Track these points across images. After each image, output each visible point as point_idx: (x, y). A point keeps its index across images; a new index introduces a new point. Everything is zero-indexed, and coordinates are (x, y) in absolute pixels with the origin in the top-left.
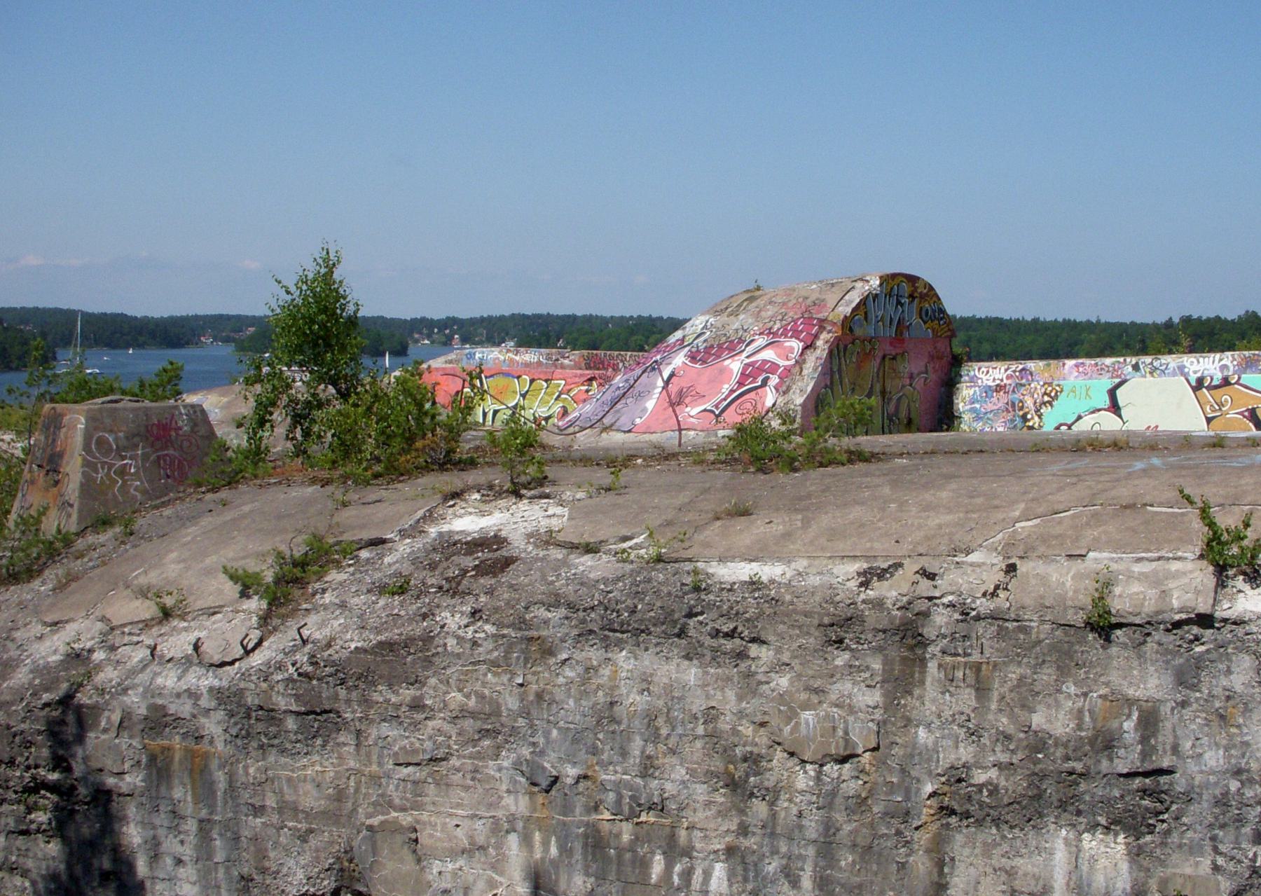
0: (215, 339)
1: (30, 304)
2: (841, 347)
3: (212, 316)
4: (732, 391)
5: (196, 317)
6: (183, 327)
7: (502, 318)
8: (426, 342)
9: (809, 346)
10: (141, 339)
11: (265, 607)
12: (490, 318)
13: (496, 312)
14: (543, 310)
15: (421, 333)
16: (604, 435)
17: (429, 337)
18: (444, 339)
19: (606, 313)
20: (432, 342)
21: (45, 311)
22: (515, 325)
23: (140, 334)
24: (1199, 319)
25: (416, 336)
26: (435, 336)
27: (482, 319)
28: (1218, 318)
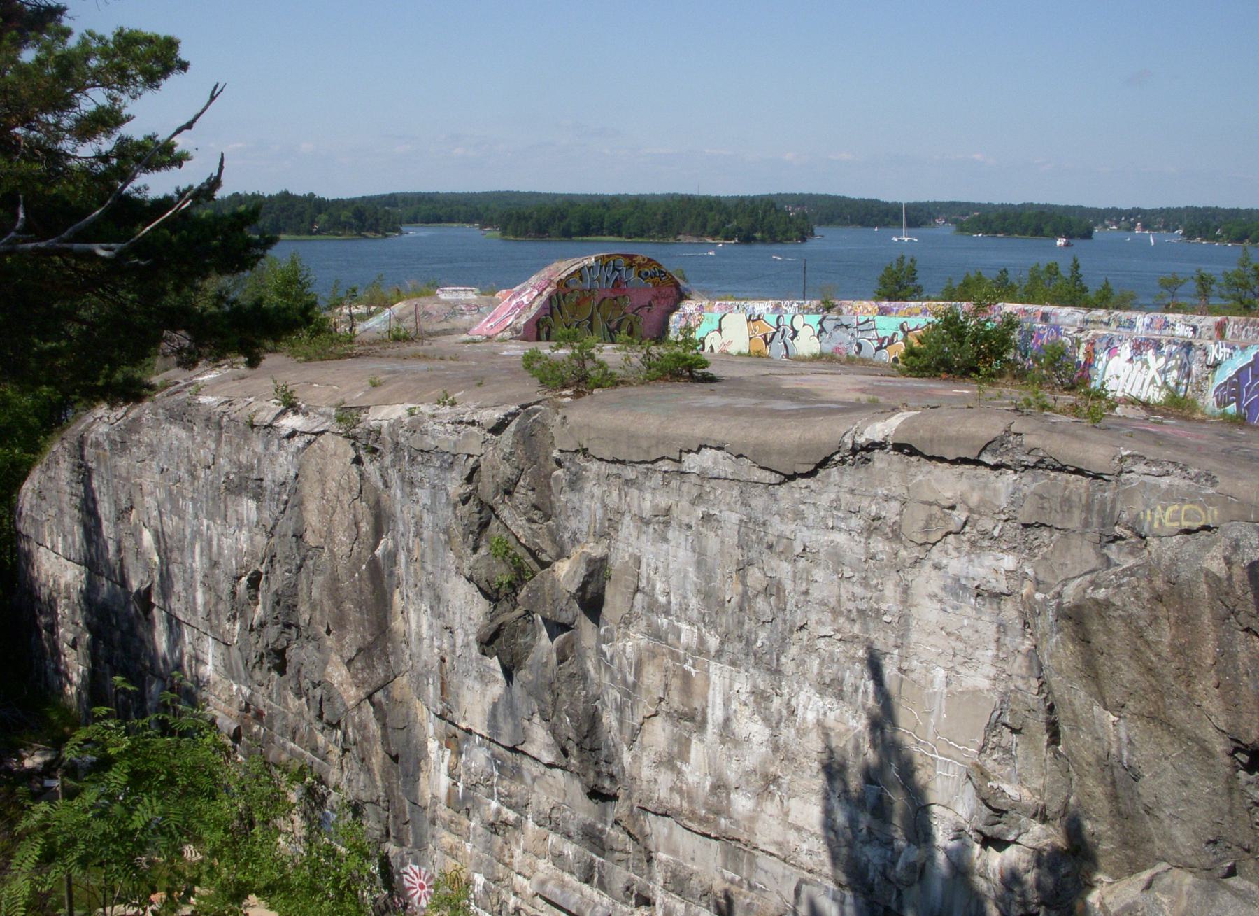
0: (947, 221)
1: (806, 191)
2: (560, 294)
3: (947, 203)
4: (165, 542)
5: (935, 203)
6: (922, 210)
7: (1178, 210)
8: (1114, 227)
9: (540, 294)
10: (887, 220)
11: (1222, 614)
12: (1169, 210)
13: (1174, 205)
14: (840, 193)
15: (1111, 220)
16: (997, 432)
17: (1117, 223)
18: (1128, 226)
19: (579, 193)
20: (1119, 228)
21: (817, 196)
22: (1188, 216)
23: (887, 215)
24: (270, 196)
25: (1107, 222)
26: (1122, 223)
27: (1162, 210)
28: (312, 195)
